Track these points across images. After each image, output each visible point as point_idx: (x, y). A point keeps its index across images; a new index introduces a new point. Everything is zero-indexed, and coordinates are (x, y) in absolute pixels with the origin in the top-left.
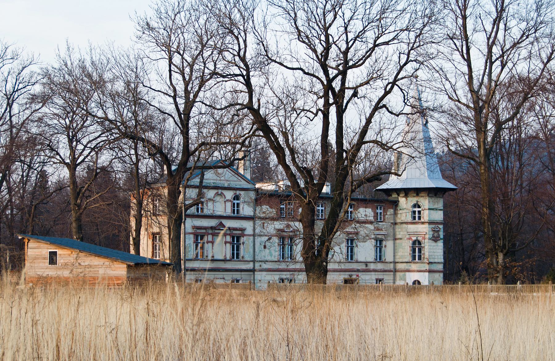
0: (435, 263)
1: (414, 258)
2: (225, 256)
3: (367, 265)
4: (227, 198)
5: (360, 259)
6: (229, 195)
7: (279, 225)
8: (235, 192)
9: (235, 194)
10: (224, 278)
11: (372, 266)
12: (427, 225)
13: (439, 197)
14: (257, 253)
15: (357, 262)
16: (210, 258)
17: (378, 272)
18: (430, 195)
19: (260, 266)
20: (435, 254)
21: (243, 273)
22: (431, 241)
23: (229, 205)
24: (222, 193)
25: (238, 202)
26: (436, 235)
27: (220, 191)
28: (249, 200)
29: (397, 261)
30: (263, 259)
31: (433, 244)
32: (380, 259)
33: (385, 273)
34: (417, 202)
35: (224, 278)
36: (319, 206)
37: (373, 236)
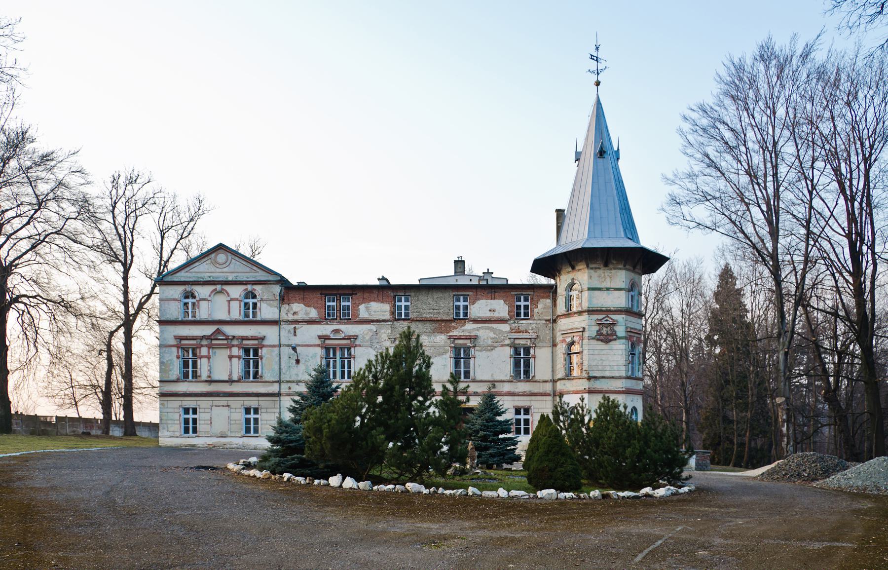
0: (603, 377)
1: (517, 373)
2: (231, 374)
3: (494, 386)
4: (233, 296)
5: (478, 378)
6: (236, 291)
7: (326, 329)
8: (244, 287)
9: (246, 289)
10: (228, 406)
11: (506, 388)
12: (585, 316)
13: (615, 269)
14: (283, 371)
15: (474, 381)
16: (204, 377)
17: (518, 395)
18: (591, 266)
19: (290, 388)
20: (605, 363)
21: (261, 398)
22: (594, 342)
23: (235, 305)
24: (222, 289)
25: (255, 301)
26: (604, 331)
27: (219, 287)
28: (271, 297)
29: (277, 343)
30: (294, 378)
31: (601, 346)
32: (256, 375)
33: (533, 398)
34: (573, 279)
35: (228, 406)
36: (400, 301)
37: (508, 342)
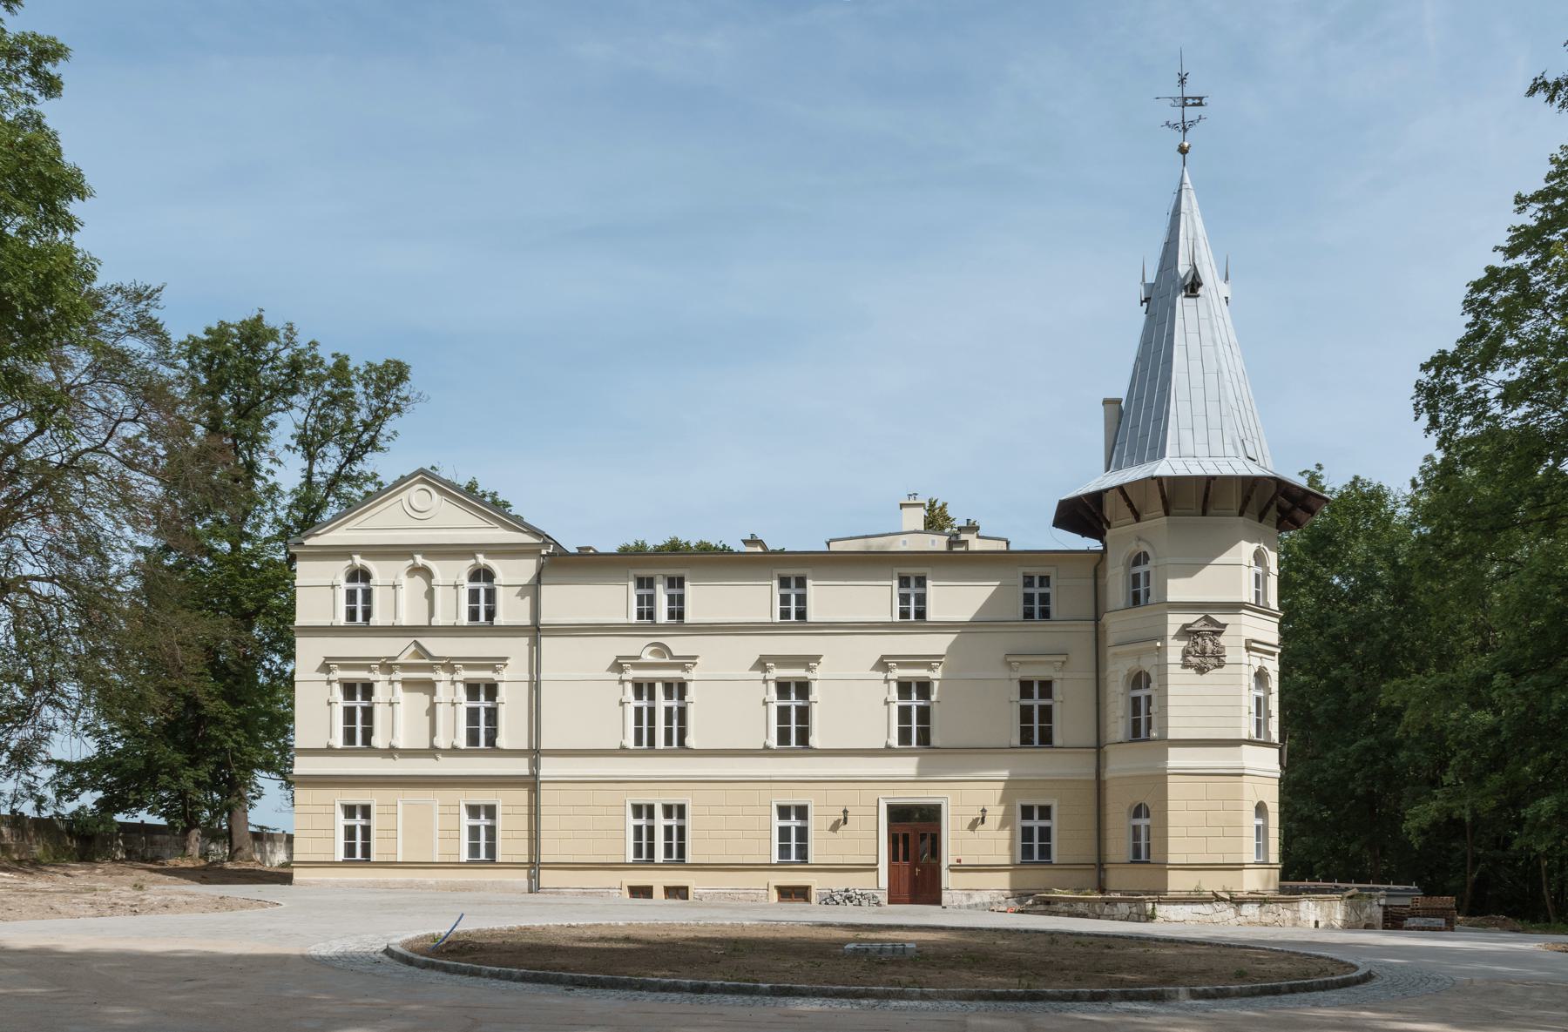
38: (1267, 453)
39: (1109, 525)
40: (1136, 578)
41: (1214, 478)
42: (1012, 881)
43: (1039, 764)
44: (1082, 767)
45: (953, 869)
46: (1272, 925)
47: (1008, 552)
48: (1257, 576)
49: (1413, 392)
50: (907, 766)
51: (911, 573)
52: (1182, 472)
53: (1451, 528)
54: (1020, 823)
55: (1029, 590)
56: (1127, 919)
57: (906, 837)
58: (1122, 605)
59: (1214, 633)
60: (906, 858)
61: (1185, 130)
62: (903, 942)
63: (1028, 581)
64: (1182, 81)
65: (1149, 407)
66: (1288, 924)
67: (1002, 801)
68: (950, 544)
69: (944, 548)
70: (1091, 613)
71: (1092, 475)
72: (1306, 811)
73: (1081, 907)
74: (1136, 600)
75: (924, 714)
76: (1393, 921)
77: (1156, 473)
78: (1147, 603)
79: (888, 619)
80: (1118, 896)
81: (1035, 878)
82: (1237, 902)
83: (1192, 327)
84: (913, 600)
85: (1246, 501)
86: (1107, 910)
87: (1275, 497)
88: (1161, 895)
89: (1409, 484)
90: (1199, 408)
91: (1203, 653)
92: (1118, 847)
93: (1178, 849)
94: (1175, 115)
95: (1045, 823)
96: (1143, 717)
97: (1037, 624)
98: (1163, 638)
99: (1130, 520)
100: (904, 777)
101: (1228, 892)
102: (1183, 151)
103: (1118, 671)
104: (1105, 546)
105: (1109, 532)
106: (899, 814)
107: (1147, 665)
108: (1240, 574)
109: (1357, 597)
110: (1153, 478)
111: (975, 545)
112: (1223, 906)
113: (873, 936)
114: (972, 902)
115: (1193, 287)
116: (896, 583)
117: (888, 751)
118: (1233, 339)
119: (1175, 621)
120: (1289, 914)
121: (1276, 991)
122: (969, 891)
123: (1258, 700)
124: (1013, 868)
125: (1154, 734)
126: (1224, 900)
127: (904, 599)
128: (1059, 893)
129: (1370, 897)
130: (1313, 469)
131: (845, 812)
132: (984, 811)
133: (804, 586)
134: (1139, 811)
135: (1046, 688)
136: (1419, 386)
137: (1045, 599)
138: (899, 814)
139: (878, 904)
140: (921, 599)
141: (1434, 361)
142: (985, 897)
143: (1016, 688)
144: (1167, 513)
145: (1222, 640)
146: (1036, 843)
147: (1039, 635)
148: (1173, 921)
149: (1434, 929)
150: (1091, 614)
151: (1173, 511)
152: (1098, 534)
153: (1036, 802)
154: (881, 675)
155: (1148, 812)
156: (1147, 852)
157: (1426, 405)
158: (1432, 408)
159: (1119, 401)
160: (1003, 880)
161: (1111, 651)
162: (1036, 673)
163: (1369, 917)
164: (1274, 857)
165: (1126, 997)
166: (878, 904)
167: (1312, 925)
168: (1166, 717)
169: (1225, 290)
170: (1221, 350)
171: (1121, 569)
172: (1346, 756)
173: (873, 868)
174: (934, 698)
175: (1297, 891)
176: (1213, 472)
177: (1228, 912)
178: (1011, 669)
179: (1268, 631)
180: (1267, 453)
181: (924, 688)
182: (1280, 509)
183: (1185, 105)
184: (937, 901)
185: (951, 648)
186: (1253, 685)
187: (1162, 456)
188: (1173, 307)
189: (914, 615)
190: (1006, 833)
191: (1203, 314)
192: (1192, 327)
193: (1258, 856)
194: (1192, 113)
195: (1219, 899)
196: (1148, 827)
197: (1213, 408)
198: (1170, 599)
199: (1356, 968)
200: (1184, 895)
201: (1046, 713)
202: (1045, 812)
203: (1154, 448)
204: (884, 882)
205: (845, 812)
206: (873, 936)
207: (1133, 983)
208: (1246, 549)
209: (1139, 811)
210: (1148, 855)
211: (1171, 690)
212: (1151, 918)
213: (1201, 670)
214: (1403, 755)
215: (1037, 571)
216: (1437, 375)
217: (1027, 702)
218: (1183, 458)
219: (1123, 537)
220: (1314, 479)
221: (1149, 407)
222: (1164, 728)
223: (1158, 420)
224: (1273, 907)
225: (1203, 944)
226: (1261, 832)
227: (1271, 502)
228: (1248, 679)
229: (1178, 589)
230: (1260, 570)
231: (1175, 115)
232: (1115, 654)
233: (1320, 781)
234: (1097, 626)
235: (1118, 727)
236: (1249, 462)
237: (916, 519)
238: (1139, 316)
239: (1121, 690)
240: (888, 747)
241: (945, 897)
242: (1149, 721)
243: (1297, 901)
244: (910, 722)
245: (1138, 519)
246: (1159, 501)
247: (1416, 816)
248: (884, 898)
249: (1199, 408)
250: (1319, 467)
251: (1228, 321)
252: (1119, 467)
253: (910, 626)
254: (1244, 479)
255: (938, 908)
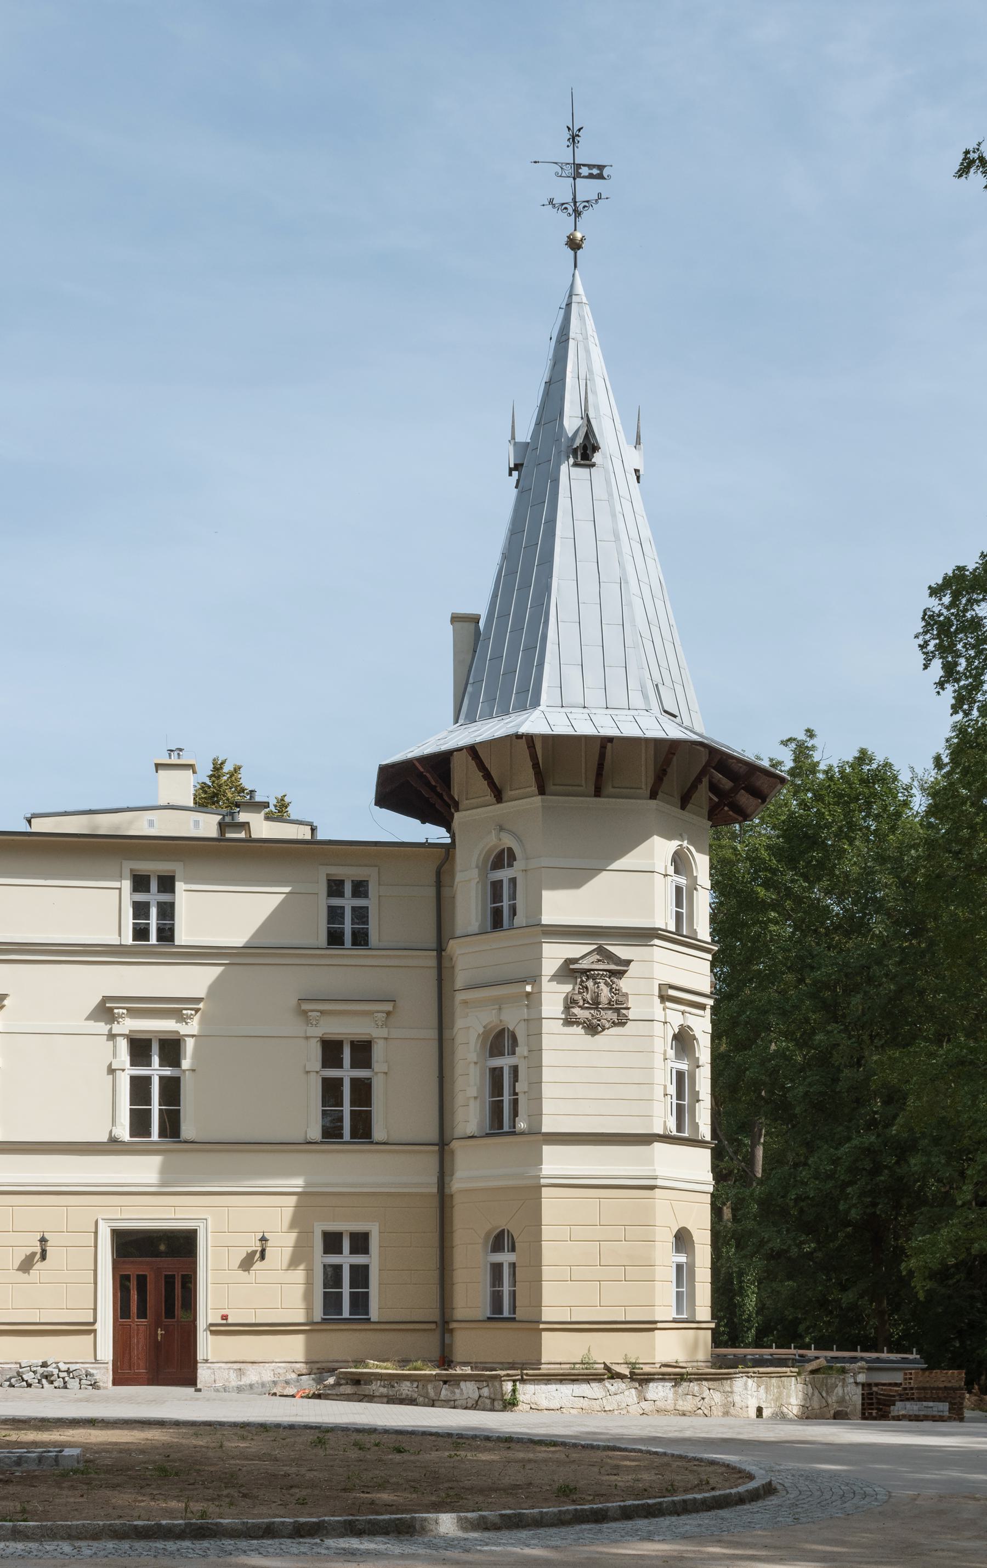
5: (459, 1318)
38: (695, 706)
39: (457, 810)
40: (496, 887)
41: (610, 739)
42: (309, 1348)
43: (351, 1169)
44: (416, 1174)
45: (215, 1330)
46: (693, 1413)
47: (313, 842)
48: (679, 890)
49: (919, 626)
50: (144, 1170)
51: (152, 870)
52: (562, 728)
53: (972, 827)
54: (320, 1259)
55: (336, 902)
56: (475, 1406)
57: (142, 1280)
58: (474, 927)
59: (613, 973)
60: (142, 1313)
61: (577, 213)
62: (62, 1445)
63: (335, 888)
64: (574, 139)
65: (517, 629)
66: (717, 1411)
67: (294, 1224)
68: (222, 826)
69: (213, 832)
70: (430, 938)
71: (435, 729)
72: (777, 1244)
73: (406, 1388)
74: (497, 921)
75: (171, 1089)
76: (876, 1407)
77: (523, 730)
78: (512, 928)
79: (113, 939)
80: (468, 1370)
81: (342, 1344)
82: (640, 1378)
83: (583, 511)
84: (154, 911)
85: (660, 776)
86: (445, 1393)
87: (703, 772)
88: (529, 1368)
89: (930, 765)
90: (591, 633)
91: (596, 1004)
92: (471, 1297)
93: (554, 1305)
94: (562, 190)
95: (359, 1260)
96: (506, 1098)
97: (348, 954)
98: (535, 979)
99: (494, 796)
100: (141, 1189)
101: (633, 1365)
102: (574, 245)
103: (470, 1027)
104: (453, 837)
105: (456, 815)
106: (129, 1244)
107: (512, 1019)
108: (651, 886)
109: (853, 926)
110: (518, 737)
111: (262, 828)
112: (618, 1385)
113: (31, 1436)
114: (245, 1381)
115: (586, 451)
116: (127, 885)
117: (112, 1146)
118: (646, 533)
119: (554, 954)
120: (717, 1397)
121: (599, 1517)
122: (240, 1365)
123: (680, 1075)
124: (310, 1328)
125: (522, 1125)
126: (621, 1376)
127: (140, 910)
128: (374, 1367)
129: (843, 1371)
130: (801, 736)
131: (43, 1240)
132: (263, 1239)
133: (172, 890)
134: (500, 1241)
135: (362, 1052)
136: (930, 620)
137: (361, 915)
138: (129, 1244)
139: (94, 1385)
140: (167, 911)
141: (948, 582)
142: (265, 1374)
143: (316, 1052)
144: (542, 792)
145: (624, 984)
146: (346, 1290)
147: (348, 971)
148: (546, 1409)
149: (935, 1419)
150: (432, 942)
151: (550, 788)
152: (445, 822)
153: (346, 1226)
154: (102, 1028)
155: (514, 1247)
156: (513, 1307)
157: (939, 647)
158: (945, 649)
159: (475, 619)
160: (294, 1348)
161: (460, 997)
162: (346, 1028)
163: (841, 1401)
164: (704, 1311)
165: (352, 1530)
166: (94, 1385)
167: (753, 1413)
168: (540, 1098)
169: (634, 459)
170: (626, 549)
171: (474, 874)
172: (836, 1161)
173: (87, 1329)
174: (186, 1064)
175: (734, 1363)
176: (609, 730)
177: (626, 1394)
178: (308, 1021)
179: (696, 973)
180: (695, 706)
181: (171, 1049)
182: (713, 788)
183: (576, 176)
184: (190, 1380)
185: (213, 988)
186: (671, 1053)
187: (536, 703)
188: (556, 481)
189: (155, 933)
190: (299, 1275)
191: (600, 491)
192: (583, 511)
193: (679, 1309)
194: (587, 189)
195: (615, 1376)
196: (513, 1266)
197: (612, 634)
198: (546, 919)
199: (751, 1477)
200: (565, 1369)
201: (362, 1091)
202: (360, 1243)
203: (523, 691)
204: (106, 1351)
205: (43, 1240)
206: (31, 1436)
207: (389, 1507)
208: (661, 849)
209: (500, 1241)
210: (513, 1309)
211: (547, 1058)
212: (510, 1404)
213: (592, 1029)
214: (915, 1162)
215: (348, 873)
216: (953, 604)
217: (333, 1073)
218: (567, 708)
219: (478, 825)
220: (802, 751)
221: (517, 629)
222: (537, 1115)
223: (530, 649)
224: (694, 1386)
225: (555, 1444)
226: (683, 1274)
227: (698, 780)
228: (662, 1043)
229: (558, 906)
230: (682, 881)
231: (562, 190)
232: (465, 1002)
233: (798, 1199)
234: (440, 958)
235: (469, 1114)
236: (665, 719)
237: (181, 789)
238: (505, 492)
239: (473, 1057)
240: (113, 1140)
241: (203, 1373)
242: (515, 1102)
243: (728, 1377)
244: (148, 1101)
245: (499, 798)
246: (531, 772)
247: (920, 1251)
248: (105, 1375)
249: (591, 633)
250: (810, 733)
251: (639, 506)
252: (471, 719)
253: (150, 952)
254: (657, 742)
255: (191, 1390)
